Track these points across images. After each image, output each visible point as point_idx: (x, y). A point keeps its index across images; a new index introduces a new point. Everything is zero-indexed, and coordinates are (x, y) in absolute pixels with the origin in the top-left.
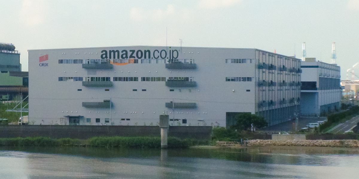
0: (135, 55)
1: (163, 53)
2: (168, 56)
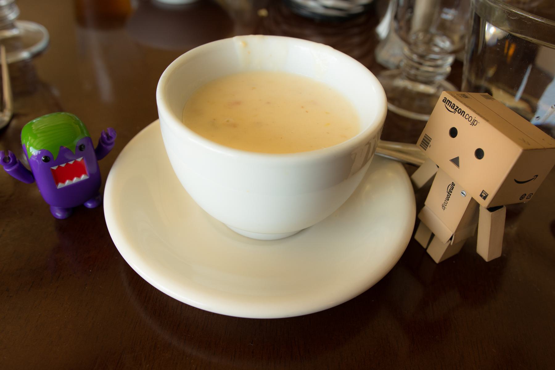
0: (457, 110)
1: (470, 118)
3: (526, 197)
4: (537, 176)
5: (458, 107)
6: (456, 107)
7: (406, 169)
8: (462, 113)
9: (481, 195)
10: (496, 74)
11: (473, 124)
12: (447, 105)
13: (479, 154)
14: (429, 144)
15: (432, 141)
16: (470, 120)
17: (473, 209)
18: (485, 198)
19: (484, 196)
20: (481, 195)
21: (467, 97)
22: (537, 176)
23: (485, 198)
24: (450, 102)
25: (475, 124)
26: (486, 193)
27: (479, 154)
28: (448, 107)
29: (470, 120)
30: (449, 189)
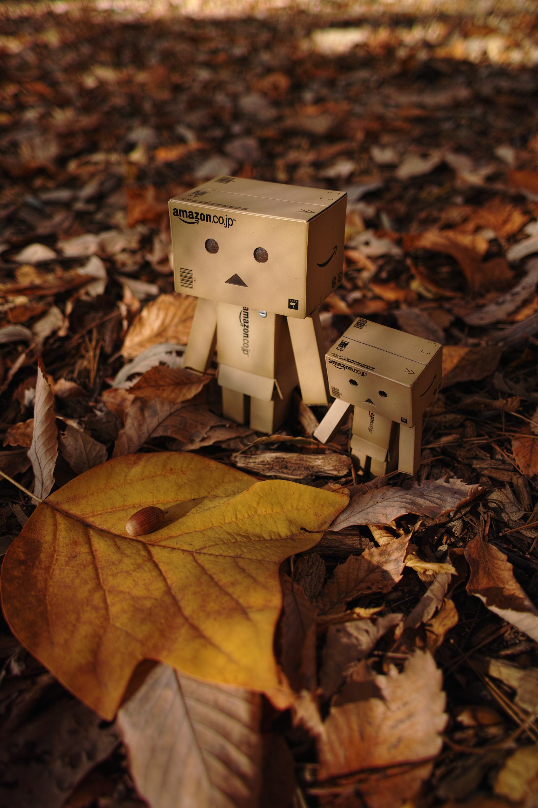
0: (199, 217)
1: (221, 219)
2: (225, 222)
3: (337, 280)
4: (336, 247)
5: (197, 214)
6: (195, 215)
7: (394, 485)
8: (207, 218)
9: (290, 307)
10: (39, 674)
11: (228, 225)
12: (182, 218)
13: (260, 255)
14: (192, 278)
15: (193, 273)
16: (221, 222)
17: (281, 323)
18: (296, 307)
19: (293, 305)
20: (290, 307)
21: (203, 193)
22: (336, 247)
23: (296, 307)
24: (183, 211)
25: (230, 223)
26: (294, 301)
27: (260, 255)
28: (185, 219)
29: (221, 222)
30: (242, 318)
